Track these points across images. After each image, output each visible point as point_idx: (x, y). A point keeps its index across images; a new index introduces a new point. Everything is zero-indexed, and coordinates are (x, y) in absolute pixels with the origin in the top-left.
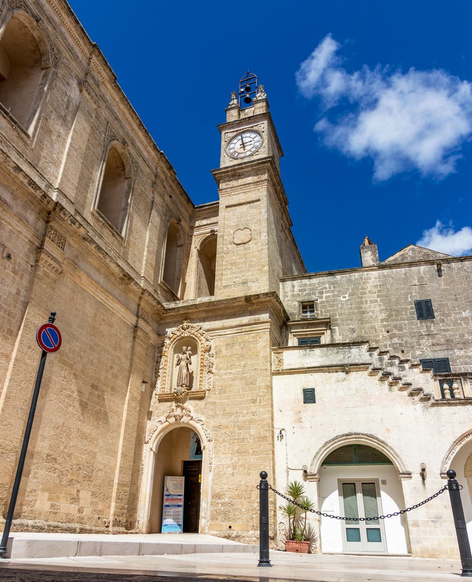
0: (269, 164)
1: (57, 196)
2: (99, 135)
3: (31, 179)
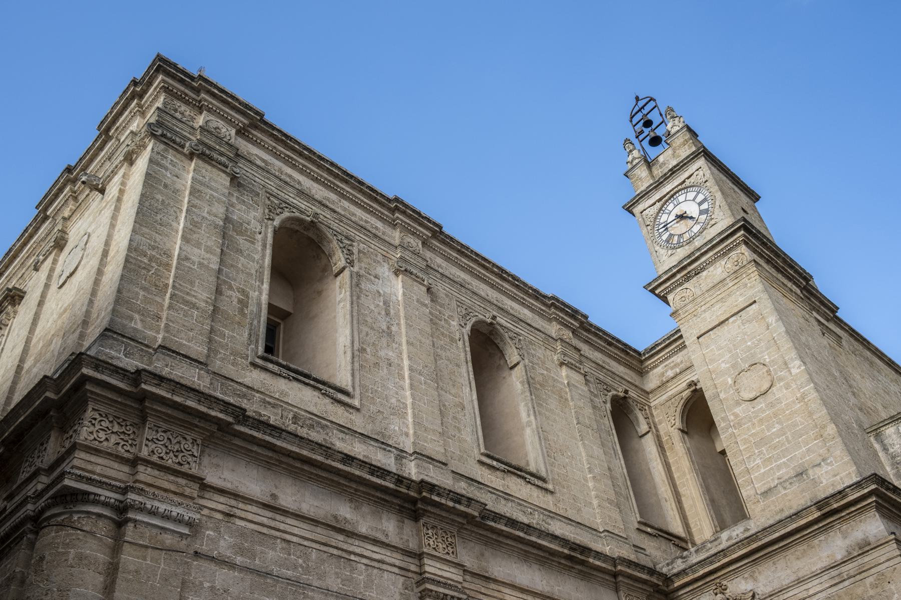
0: (742, 232)
1: (418, 466)
2: (447, 326)
3: (371, 465)
